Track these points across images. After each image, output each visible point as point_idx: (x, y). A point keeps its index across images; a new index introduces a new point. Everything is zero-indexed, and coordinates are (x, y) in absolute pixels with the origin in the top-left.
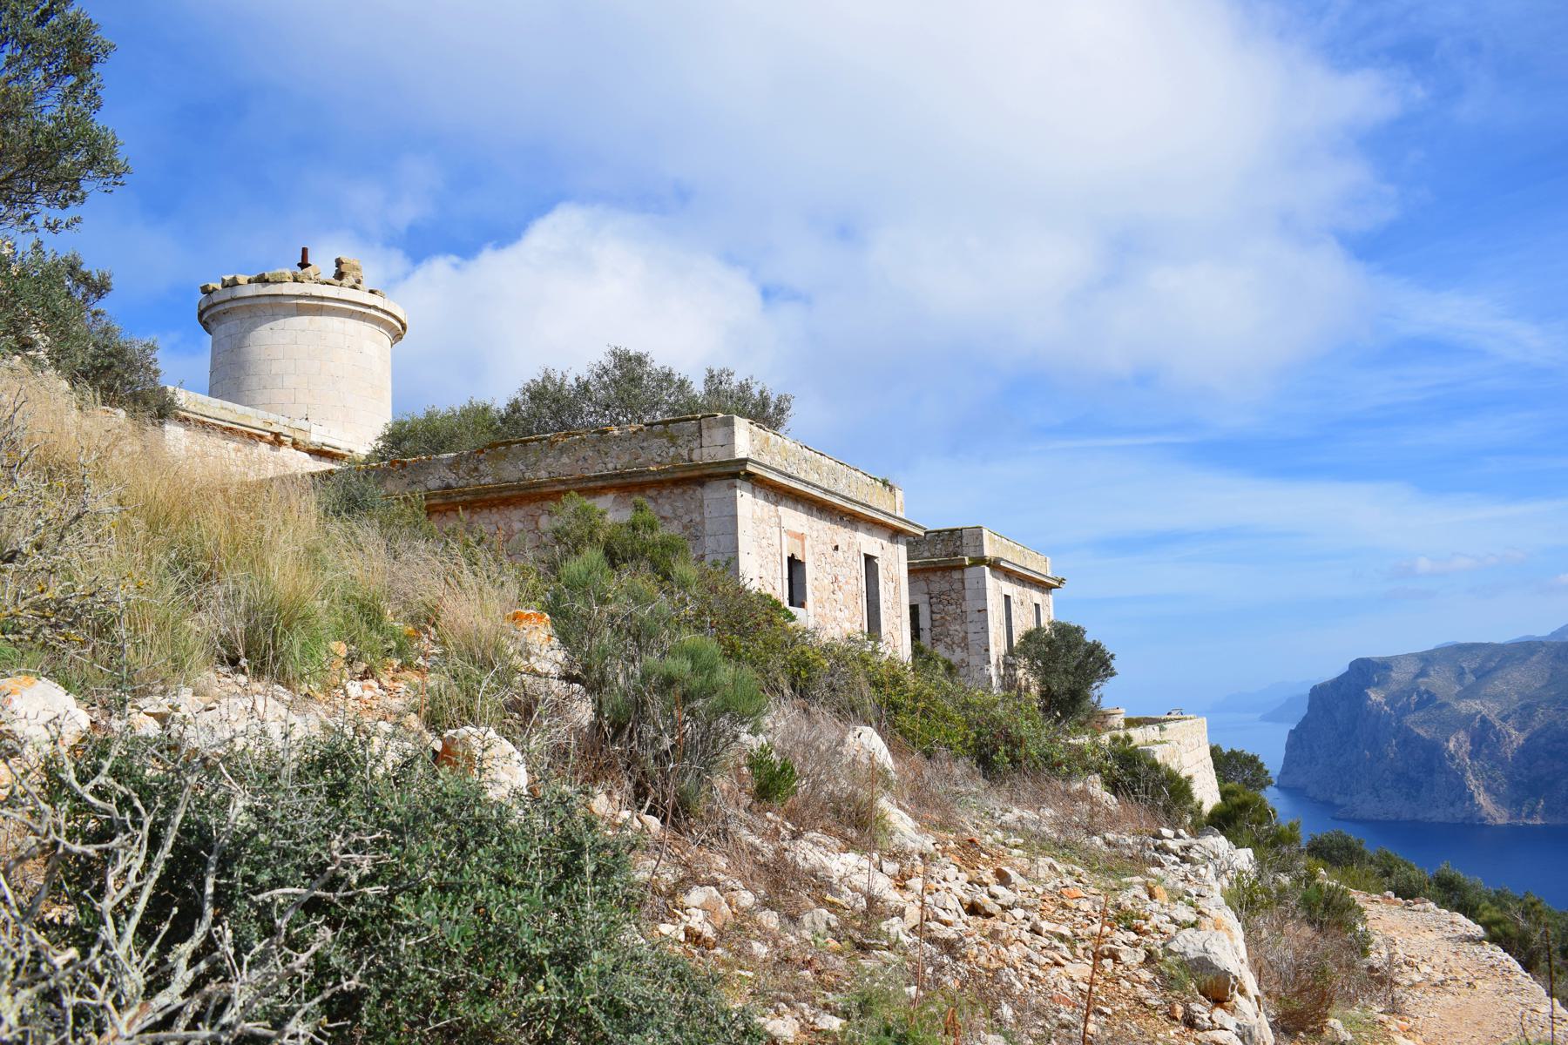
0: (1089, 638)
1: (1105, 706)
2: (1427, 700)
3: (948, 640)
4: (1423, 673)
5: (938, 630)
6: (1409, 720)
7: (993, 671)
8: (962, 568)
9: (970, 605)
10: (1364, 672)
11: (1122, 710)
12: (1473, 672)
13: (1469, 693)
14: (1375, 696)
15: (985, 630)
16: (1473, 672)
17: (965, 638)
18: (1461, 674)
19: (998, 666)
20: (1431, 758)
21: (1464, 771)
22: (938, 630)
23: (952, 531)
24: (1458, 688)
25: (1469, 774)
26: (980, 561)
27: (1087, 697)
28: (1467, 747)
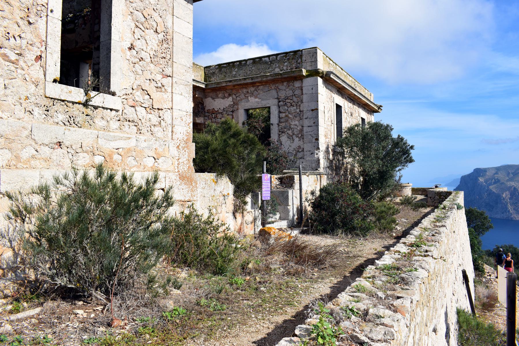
0: (394, 135)
1: (403, 181)
2: (497, 181)
3: (290, 132)
4: (496, 173)
5: (283, 125)
6: (491, 187)
7: (321, 155)
8: (301, 78)
9: (305, 106)
10: (478, 172)
11: (410, 184)
12: (512, 173)
13: (511, 180)
14: (481, 180)
15: (316, 124)
16: (512, 173)
17: (302, 130)
18: (508, 174)
19: (327, 152)
20: (498, 198)
21: (507, 204)
22: (283, 125)
23: (295, 52)
24: (507, 178)
25: (509, 204)
26: (315, 73)
27: (392, 176)
28: (509, 196)
